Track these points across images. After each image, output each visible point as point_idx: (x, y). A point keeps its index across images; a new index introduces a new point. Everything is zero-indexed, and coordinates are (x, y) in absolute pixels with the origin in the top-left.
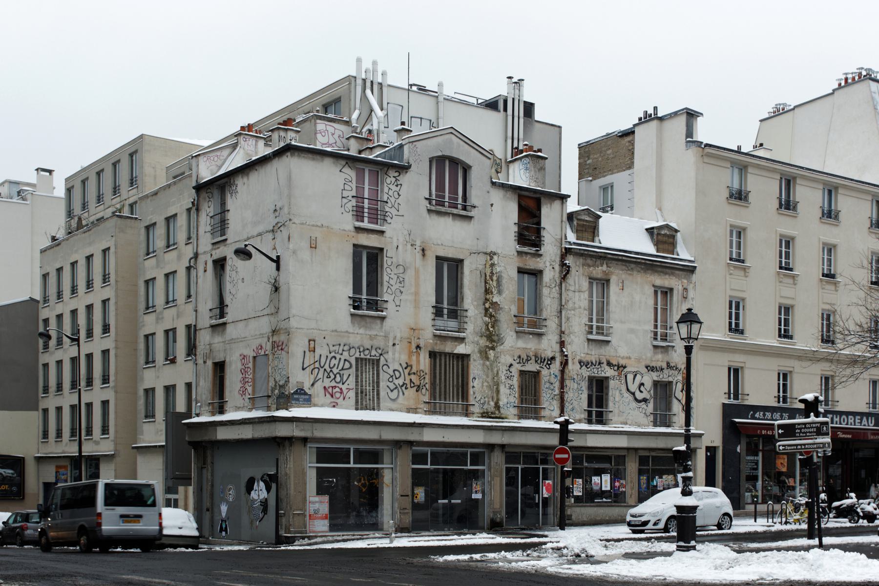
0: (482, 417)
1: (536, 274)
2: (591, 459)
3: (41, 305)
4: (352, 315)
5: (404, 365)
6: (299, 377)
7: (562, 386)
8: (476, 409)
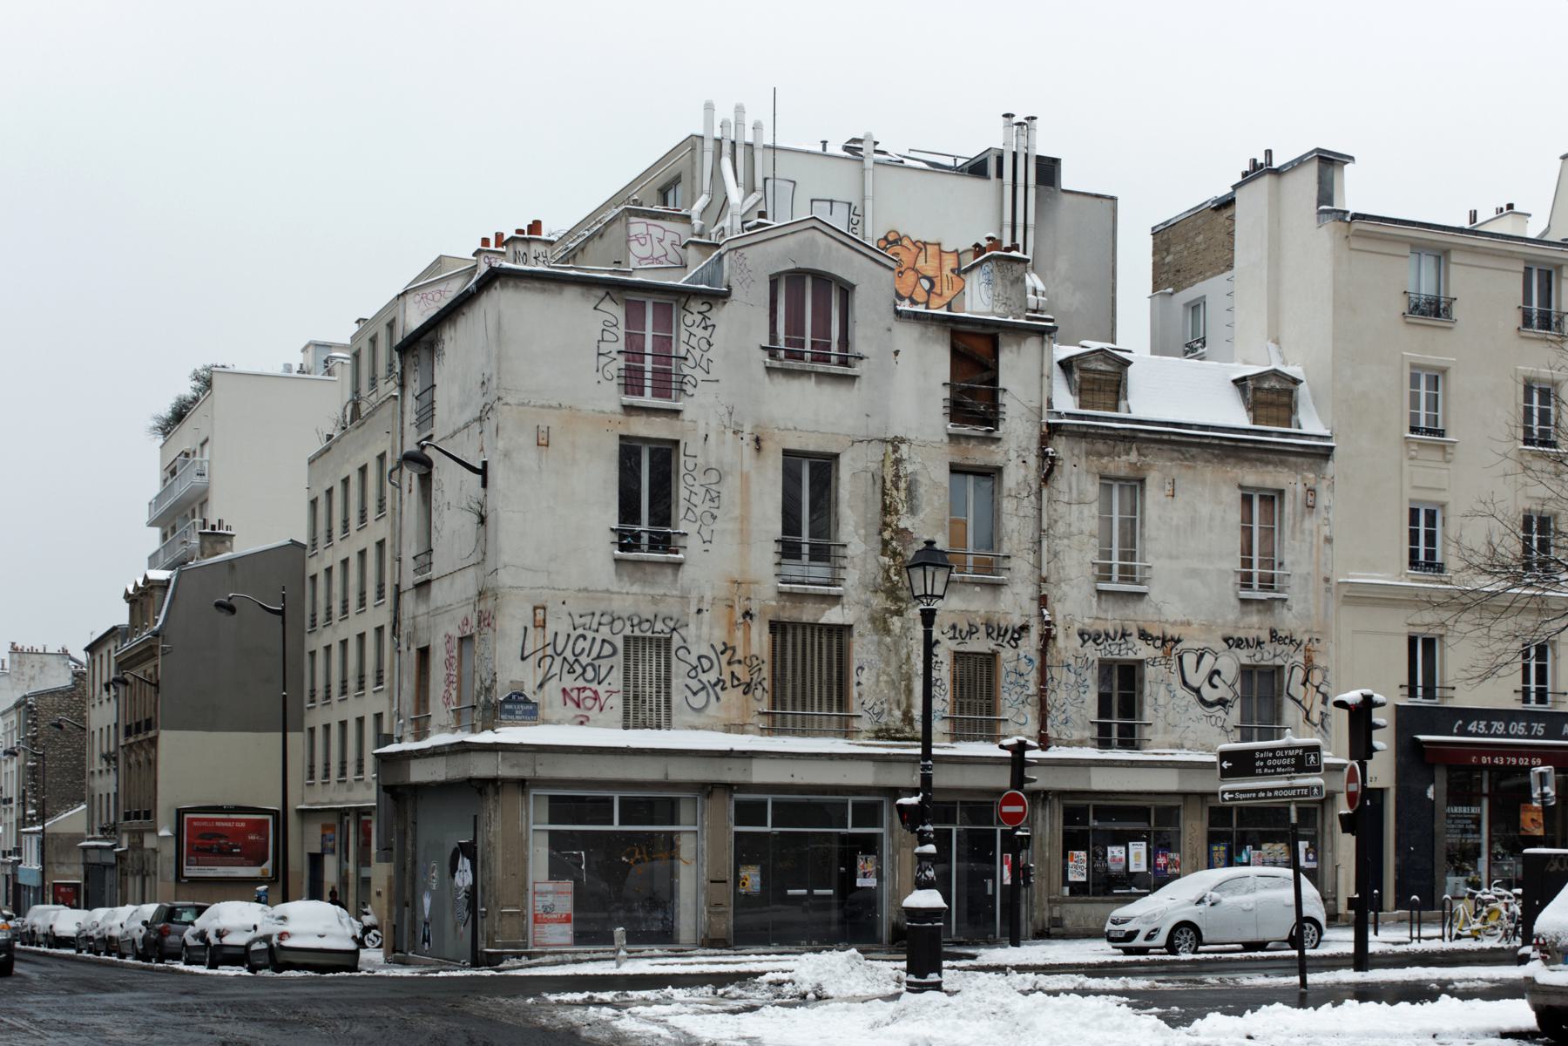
0: (878, 738)
1: (992, 474)
2: (1103, 813)
3: (308, 553)
4: (617, 561)
5: (720, 648)
6: (512, 670)
7: (1043, 680)
8: (865, 724)
